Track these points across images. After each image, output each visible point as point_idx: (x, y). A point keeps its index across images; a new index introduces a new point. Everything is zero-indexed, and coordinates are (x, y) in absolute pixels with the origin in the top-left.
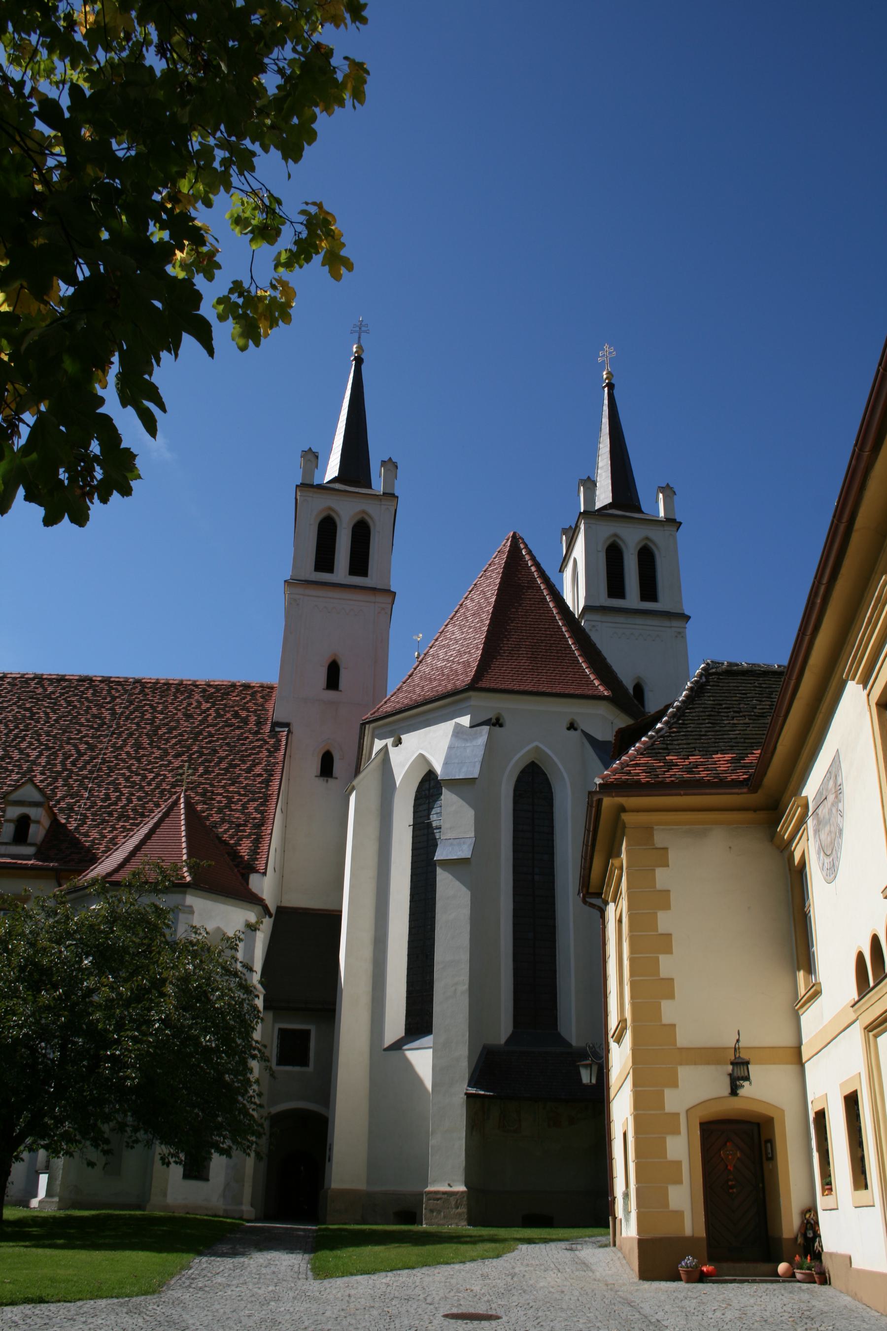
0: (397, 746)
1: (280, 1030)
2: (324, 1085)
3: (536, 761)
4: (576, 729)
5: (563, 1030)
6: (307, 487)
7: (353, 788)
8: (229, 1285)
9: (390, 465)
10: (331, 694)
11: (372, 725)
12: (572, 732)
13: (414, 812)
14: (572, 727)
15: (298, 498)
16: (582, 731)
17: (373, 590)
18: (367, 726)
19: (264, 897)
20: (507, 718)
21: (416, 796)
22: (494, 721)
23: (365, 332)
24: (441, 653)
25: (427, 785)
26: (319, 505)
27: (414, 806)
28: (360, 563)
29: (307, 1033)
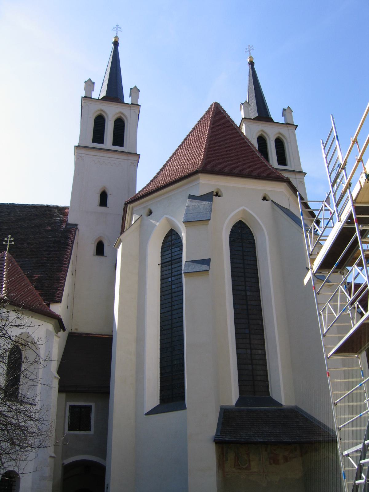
0: (149, 215)
1: (72, 407)
2: (102, 444)
3: (243, 220)
4: (267, 200)
5: (274, 395)
6: (87, 98)
7: (120, 241)
8: (9, 453)
9: (135, 91)
10: (103, 209)
11: (132, 205)
12: (265, 201)
13: (162, 256)
14: (265, 199)
15: (83, 105)
16: (272, 201)
17: (127, 153)
18: (129, 205)
19: (61, 317)
20: (224, 192)
21: (162, 246)
22: (215, 193)
23: (120, 31)
24: (175, 164)
25: (170, 239)
26: (94, 110)
27: (161, 253)
28: (119, 139)
29: (90, 408)
